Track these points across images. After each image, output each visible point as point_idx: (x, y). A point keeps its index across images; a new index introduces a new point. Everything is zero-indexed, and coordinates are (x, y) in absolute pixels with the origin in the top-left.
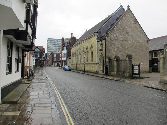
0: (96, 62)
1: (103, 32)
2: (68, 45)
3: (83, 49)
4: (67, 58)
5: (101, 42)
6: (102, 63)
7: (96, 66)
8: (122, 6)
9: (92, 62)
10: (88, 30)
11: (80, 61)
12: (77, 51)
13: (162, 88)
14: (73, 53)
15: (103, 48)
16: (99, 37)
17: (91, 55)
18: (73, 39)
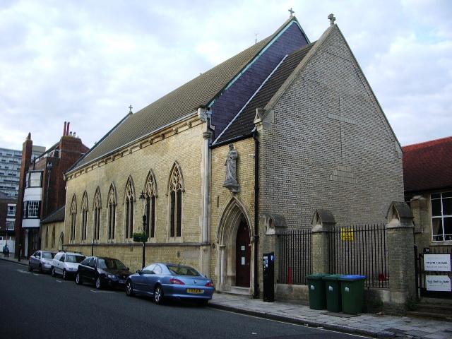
1: (232, 108)
3: (130, 182)
5: (232, 148)
6: (231, 242)
8: (296, 20)
9: (179, 240)
10: (134, 113)
11: (96, 236)
13: (396, 325)
14: (74, 198)
16: (213, 128)
17: (168, 207)
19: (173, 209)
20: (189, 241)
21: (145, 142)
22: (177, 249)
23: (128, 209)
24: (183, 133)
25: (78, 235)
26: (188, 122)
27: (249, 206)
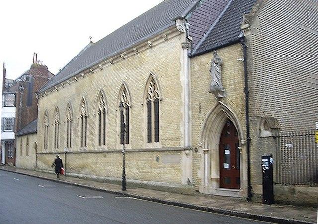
0: (184, 143)
2: (23, 91)
4: (20, 133)
5: (215, 55)
7: (186, 160)
9: (158, 145)
11: (69, 144)
12: (69, 105)
14: (46, 113)
15: (227, 82)
17: (145, 115)
18: (39, 71)
19: (149, 117)
20: (169, 146)
21: (117, 58)
22: (155, 154)
23: (100, 120)
24: (158, 46)
25: (51, 144)
26: (164, 35)
27: (238, 110)
